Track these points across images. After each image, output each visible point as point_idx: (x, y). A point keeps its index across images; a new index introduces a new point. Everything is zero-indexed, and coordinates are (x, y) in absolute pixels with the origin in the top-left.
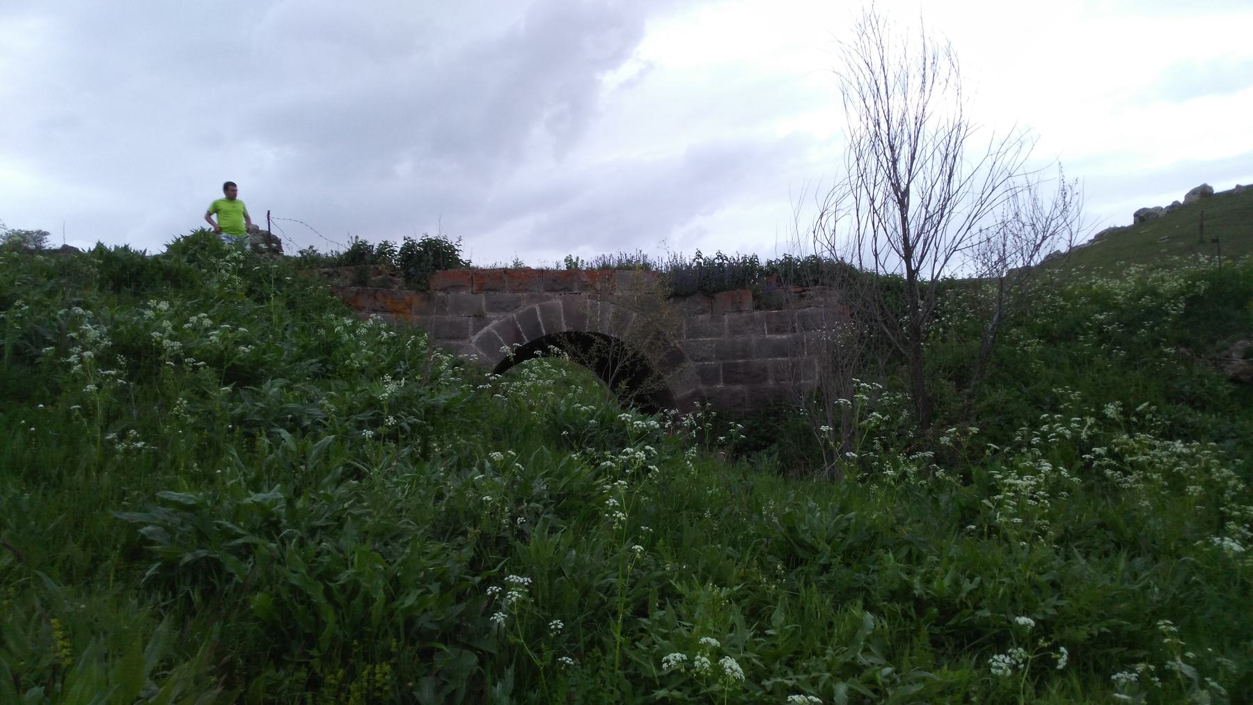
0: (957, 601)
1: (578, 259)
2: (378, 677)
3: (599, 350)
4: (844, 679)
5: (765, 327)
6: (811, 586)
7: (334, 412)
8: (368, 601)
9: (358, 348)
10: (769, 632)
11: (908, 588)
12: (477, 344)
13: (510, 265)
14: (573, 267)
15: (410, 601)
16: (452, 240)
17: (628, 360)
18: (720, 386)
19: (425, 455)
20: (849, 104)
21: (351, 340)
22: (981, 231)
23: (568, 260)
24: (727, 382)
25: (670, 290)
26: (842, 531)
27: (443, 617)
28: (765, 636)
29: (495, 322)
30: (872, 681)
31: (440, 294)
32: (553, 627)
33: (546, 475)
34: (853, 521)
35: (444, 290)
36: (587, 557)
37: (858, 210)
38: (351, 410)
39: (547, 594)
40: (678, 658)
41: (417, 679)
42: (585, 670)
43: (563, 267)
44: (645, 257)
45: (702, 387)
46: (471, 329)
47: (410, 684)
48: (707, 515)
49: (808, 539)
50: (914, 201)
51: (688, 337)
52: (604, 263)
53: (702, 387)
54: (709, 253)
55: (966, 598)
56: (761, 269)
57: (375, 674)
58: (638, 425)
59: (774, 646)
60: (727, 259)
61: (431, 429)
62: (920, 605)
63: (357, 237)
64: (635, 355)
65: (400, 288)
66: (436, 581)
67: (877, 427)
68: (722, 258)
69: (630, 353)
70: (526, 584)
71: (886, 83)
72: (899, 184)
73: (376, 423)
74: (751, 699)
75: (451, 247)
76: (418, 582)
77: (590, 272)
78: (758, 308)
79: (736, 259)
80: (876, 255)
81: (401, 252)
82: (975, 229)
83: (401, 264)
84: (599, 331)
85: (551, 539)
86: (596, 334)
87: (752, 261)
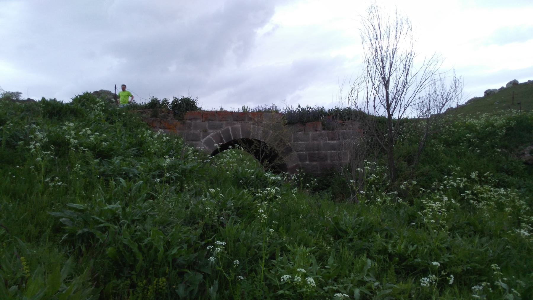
1: (247, 107)
2: (160, 283)
3: (256, 146)
6: (345, 248)
8: (157, 251)
11: (386, 249)
12: (204, 143)
13: (219, 109)
14: (245, 111)
15: (174, 251)
16: (194, 98)
18: (307, 162)
19: (182, 190)
20: (364, 43)
23: (243, 108)
24: (310, 161)
25: (287, 121)
27: (188, 258)
29: (212, 134)
30: (370, 288)
31: (189, 121)
32: (235, 263)
34: (363, 220)
35: (190, 120)
38: (150, 170)
40: (288, 277)
42: (248, 282)
43: (241, 111)
44: (276, 107)
45: (299, 163)
46: (202, 136)
47: (174, 287)
49: (344, 228)
50: (392, 85)
51: (294, 141)
52: (259, 109)
53: (299, 163)
54: (304, 106)
56: (326, 113)
58: (272, 178)
59: (329, 273)
60: (311, 108)
61: (184, 179)
63: (153, 97)
64: (271, 149)
65: (172, 119)
66: (186, 243)
67: (374, 181)
68: (309, 108)
69: (269, 148)
72: (385, 78)
73: (160, 176)
75: (193, 101)
76: (178, 244)
77: (253, 113)
78: (324, 129)
79: (315, 109)
80: (375, 108)
81: (172, 103)
82: (417, 97)
86: (255, 140)
87: (322, 110)
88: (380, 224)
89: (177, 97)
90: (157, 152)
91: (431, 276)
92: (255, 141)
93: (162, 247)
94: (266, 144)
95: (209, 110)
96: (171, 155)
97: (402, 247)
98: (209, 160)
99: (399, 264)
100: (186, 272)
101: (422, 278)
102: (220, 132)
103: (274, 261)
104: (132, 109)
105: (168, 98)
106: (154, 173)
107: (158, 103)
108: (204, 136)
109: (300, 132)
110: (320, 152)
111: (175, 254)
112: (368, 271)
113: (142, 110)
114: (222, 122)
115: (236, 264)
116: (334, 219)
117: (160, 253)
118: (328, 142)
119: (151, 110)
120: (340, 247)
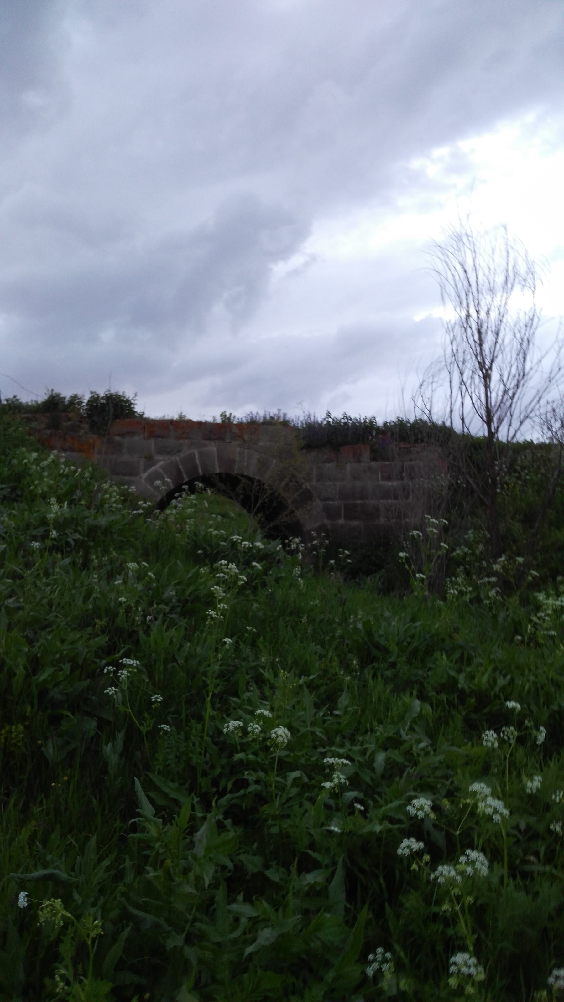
0: (492, 694)
1: (231, 414)
2: (13, 735)
3: (244, 489)
4: (385, 749)
5: (380, 476)
6: (377, 678)
7: (14, 528)
8: (11, 674)
9: (41, 478)
10: (336, 712)
11: (455, 682)
12: (146, 480)
13: (176, 417)
14: (227, 421)
15: (43, 676)
16: (129, 395)
17: (267, 498)
18: (342, 521)
19: (86, 565)
20: (446, 296)
21: (37, 471)
22: (548, 403)
23: (223, 415)
24: (347, 518)
25: (303, 442)
26: (410, 637)
27: (71, 690)
28: (332, 714)
29: (161, 463)
30: (408, 753)
31: (118, 438)
32: (153, 700)
33: (179, 584)
34: (418, 629)
35: (122, 435)
36: (199, 650)
37: (451, 382)
38: (28, 526)
39: (162, 676)
40: (236, 725)
41: (46, 738)
42: (179, 736)
43: (219, 420)
44: (285, 415)
45: (326, 521)
46: (142, 467)
47: (40, 742)
48: (304, 619)
49: (383, 642)
50: (495, 376)
51: (318, 481)
52: (252, 418)
53: (326, 521)
54: (337, 414)
55: (499, 692)
56: (378, 429)
57: (11, 733)
58: (245, 545)
59: (339, 724)
60: (351, 419)
61: (92, 544)
62: (463, 696)
63: (52, 390)
64: (272, 494)
65: (86, 433)
66: (69, 662)
67: (464, 558)
68: (347, 418)
69: (269, 492)
70: (135, 665)
71: (477, 282)
72: (484, 362)
73: (44, 537)
74: (309, 763)
75: (128, 401)
76: (55, 662)
77: (240, 425)
78: (374, 459)
79: (359, 420)
80: (463, 420)
81: (87, 404)
82: (543, 402)
83: (87, 414)
84: (245, 474)
85: (168, 633)
86: (242, 475)
87: (371, 422)
88: (451, 637)
89: (98, 393)
90: (46, 492)
91: (508, 729)
92: (242, 478)
93: (21, 667)
94: (263, 484)
95: (158, 419)
96: (74, 499)
97: (485, 679)
98: (141, 511)
99: (476, 710)
100: (67, 716)
101: (484, 732)
102: (178, 459)
103: (235, 699)
104: (11, 412)
105: (80, 393)
106: (34, 533)
107: (62, 402)
108: (146, 468)
109: (329, 462)
110: (367, 501)
111: (45, 681)
112: (414, 721)
113: (30, 415)
114: (182, 441)
115: (156, 702)
116: (366, 624)
117: (16, 678)
118: (381, 483)
119: (48, 414)
120: (369, 677)
